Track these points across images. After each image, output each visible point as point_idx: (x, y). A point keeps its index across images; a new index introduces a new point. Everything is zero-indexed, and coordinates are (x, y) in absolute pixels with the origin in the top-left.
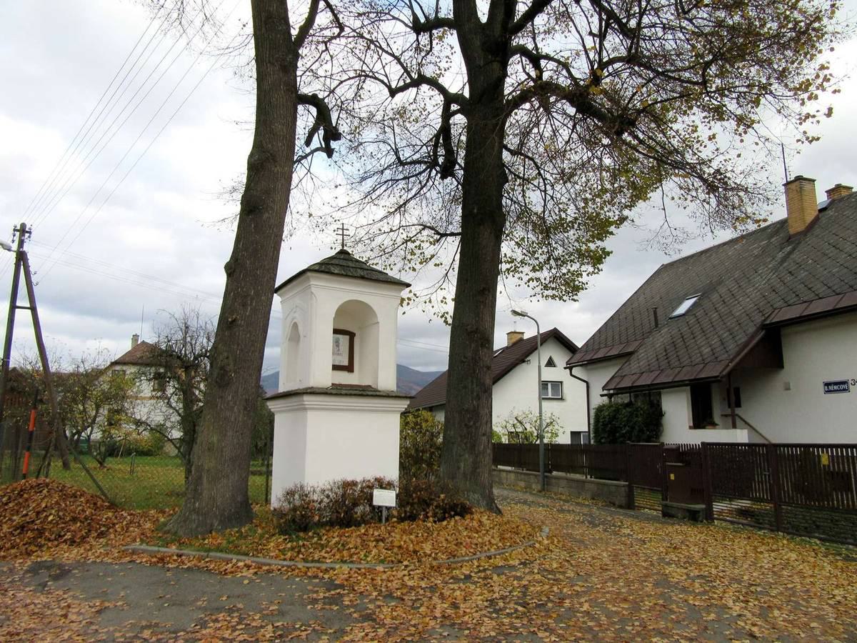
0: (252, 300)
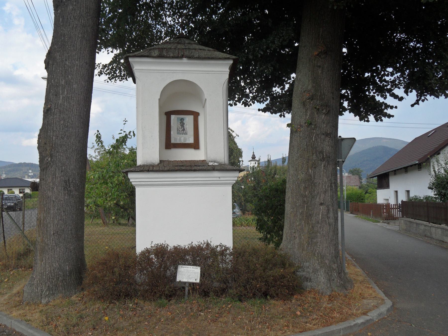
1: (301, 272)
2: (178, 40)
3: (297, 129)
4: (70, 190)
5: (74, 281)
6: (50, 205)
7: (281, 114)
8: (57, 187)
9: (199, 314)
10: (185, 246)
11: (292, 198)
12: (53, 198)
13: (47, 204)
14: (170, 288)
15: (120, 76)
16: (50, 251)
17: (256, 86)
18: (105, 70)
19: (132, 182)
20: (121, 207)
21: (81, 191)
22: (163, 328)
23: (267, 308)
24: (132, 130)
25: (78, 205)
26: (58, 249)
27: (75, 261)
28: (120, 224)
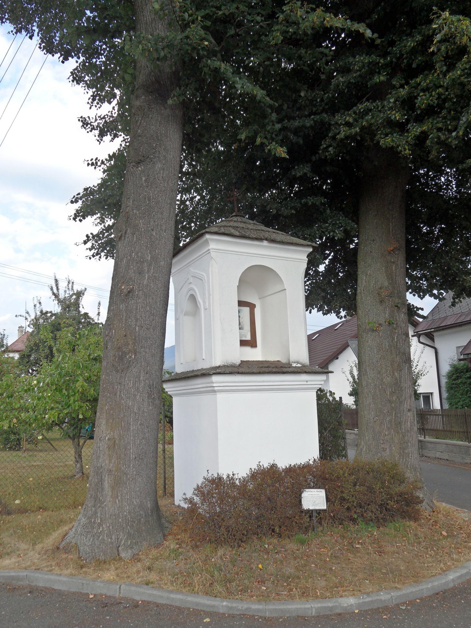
0: (150, 265)
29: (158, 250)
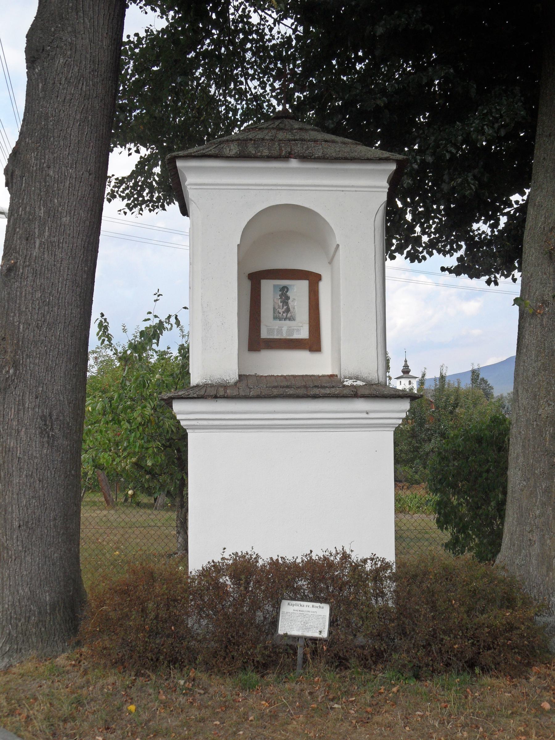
1: (544, 616)
2: (277, 122)
3: (535, 308)
4: (52, 435)
5: (60, 625)
6: (12, 466)
7: (490, 279)
8: (27, 429)
9: (329, 707)
10: (295, 558)
11: (524, 457)
12: (18, 452)
13: (6, 465)
14: (266, 648)
15: (151, 200)
16: (13, 561)
17: (435, 220)
18: (121, 189)
19: (182, 420)
20: (146, 471)
21: (75, 437)
22: (254, 735)
23: (476, 694)
24: (173, 314)
25: (69, 467)
26: (28, 559)
27: (62, 583)
28: (138, 504)
29: (57, 199)
